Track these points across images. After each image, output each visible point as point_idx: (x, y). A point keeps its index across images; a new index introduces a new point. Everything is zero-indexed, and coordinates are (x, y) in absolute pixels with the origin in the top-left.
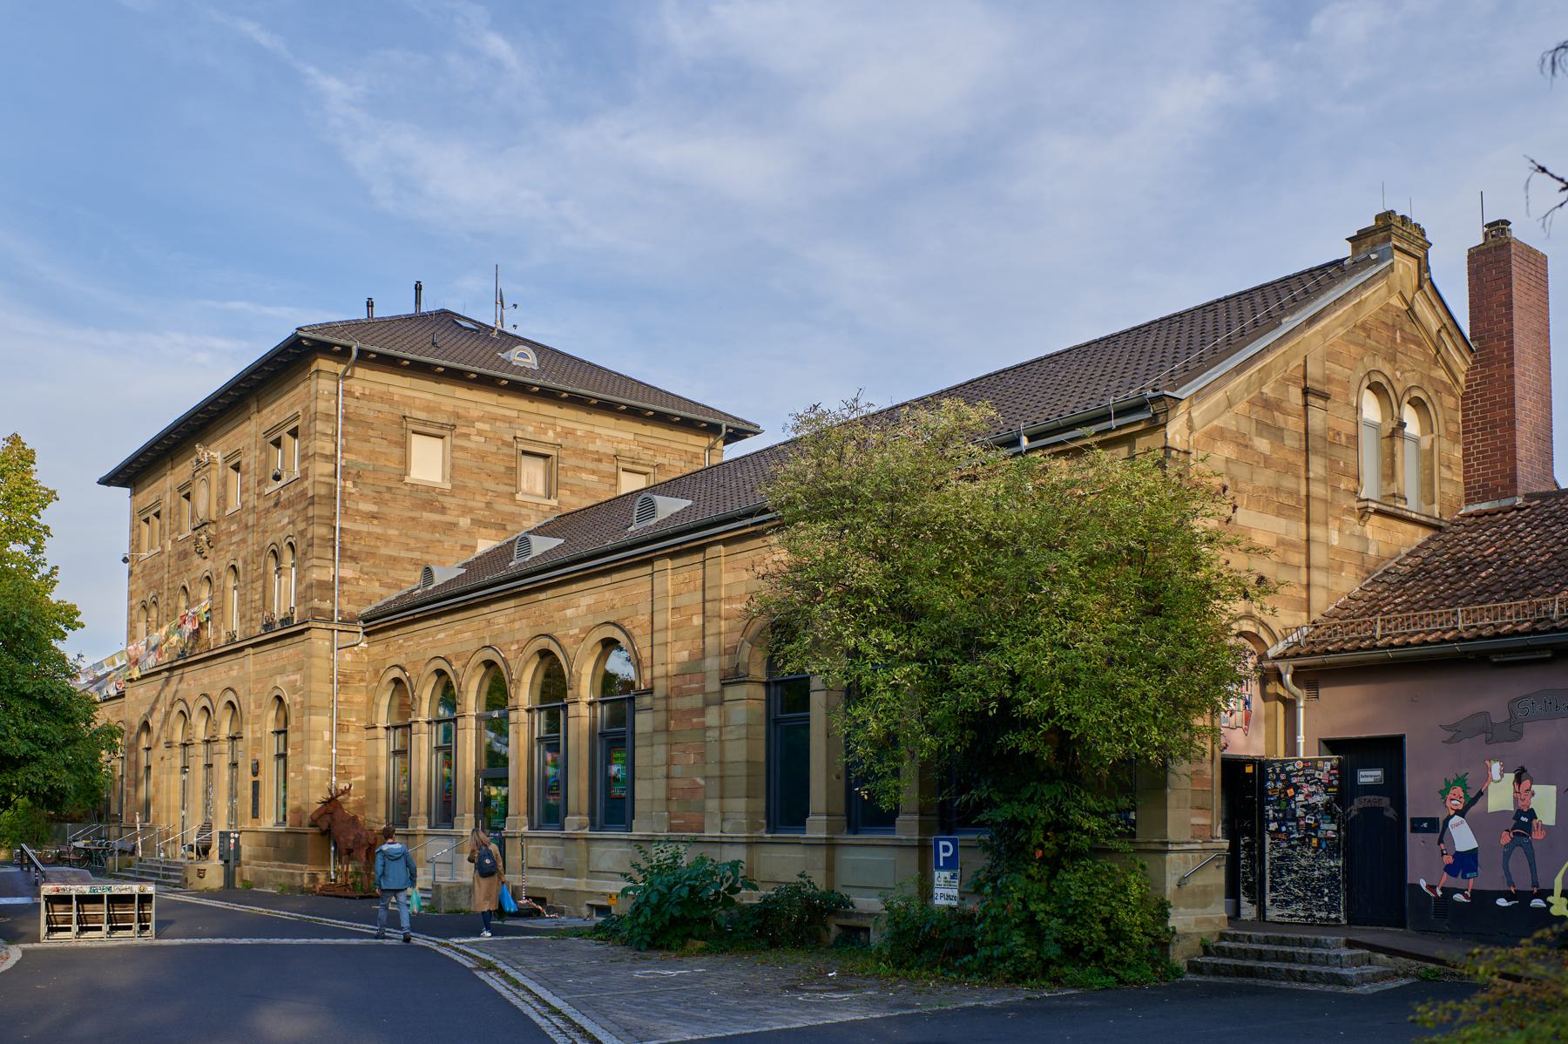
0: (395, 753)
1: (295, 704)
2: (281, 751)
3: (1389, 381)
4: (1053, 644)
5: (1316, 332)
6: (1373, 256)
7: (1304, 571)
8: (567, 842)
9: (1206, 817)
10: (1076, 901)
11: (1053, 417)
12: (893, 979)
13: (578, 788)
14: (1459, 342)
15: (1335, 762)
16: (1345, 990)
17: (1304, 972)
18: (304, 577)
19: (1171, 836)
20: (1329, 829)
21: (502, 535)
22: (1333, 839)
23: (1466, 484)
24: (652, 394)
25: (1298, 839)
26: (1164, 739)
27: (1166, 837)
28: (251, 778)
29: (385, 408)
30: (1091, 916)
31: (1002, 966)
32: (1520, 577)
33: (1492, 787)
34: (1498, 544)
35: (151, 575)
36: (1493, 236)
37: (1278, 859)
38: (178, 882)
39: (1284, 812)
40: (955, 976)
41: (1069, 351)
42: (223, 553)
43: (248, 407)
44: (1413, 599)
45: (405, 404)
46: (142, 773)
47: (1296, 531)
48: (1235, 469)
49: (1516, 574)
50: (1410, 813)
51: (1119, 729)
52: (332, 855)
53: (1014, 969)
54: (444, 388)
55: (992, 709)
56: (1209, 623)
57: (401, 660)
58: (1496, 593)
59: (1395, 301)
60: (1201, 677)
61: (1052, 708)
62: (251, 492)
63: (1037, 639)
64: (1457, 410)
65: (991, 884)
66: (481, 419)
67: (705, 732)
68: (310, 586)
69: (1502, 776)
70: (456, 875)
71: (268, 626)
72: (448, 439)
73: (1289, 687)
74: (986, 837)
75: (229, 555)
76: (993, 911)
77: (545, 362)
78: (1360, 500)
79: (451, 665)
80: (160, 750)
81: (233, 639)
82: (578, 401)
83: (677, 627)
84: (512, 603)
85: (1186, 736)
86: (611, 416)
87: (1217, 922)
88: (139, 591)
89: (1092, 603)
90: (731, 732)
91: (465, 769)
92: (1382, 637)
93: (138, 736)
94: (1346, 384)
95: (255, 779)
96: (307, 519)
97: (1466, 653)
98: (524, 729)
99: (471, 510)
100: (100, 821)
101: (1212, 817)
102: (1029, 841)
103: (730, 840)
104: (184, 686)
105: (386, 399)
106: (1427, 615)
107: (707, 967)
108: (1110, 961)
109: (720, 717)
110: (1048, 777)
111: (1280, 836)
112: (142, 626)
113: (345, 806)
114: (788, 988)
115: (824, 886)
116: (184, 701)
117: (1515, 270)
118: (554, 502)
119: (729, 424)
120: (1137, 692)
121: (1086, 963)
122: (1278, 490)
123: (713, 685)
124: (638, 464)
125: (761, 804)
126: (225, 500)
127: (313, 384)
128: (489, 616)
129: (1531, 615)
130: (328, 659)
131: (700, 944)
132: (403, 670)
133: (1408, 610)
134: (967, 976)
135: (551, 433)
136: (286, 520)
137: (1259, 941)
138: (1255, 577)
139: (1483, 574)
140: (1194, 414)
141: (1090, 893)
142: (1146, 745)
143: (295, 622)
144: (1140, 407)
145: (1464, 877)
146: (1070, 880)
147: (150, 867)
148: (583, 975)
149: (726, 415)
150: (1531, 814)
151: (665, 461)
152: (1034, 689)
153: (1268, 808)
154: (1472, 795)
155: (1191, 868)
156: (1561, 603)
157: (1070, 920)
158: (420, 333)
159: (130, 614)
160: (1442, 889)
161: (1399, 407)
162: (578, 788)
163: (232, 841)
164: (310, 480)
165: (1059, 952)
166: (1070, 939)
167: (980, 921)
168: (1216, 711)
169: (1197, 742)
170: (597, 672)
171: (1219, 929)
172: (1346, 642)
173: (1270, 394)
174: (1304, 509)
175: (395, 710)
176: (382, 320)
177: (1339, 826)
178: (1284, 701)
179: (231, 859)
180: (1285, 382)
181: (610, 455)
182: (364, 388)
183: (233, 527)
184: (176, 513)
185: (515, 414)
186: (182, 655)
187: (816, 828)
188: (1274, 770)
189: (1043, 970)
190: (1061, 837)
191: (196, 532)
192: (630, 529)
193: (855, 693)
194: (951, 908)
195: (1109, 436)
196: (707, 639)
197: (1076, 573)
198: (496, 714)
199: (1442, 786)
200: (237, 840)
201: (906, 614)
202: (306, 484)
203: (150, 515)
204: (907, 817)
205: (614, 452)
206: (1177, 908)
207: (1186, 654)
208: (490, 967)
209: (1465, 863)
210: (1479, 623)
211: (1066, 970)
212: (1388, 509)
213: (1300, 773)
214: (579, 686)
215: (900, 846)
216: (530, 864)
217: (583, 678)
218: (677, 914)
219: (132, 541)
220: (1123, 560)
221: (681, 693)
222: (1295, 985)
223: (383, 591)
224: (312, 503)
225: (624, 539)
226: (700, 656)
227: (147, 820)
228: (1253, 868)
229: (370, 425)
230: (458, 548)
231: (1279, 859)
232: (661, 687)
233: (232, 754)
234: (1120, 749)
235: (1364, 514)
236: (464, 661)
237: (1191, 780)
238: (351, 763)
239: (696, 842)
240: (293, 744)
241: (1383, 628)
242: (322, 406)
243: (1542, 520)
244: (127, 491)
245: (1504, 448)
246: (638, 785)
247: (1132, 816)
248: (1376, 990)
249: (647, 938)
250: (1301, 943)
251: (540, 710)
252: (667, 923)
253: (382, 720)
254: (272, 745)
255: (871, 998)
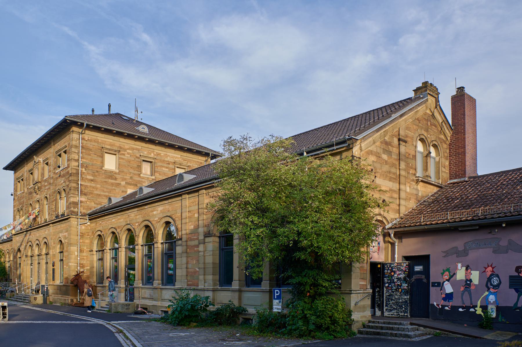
0: (99, 259)
1: (66, 243)
2: (62, 258)
3: (426, 138)
4: (312, 222)
5: (403, 120)
6: (421, 96)
7: (398, 200)
8: (154, 289)
9: (365, 282)
10: (320, 310)
11: (315, 145)
12: (258, 337)
13: (158, 271)
14: (448, 126)
15: (407, 264)
16: (409, 340)
17: (396, 334)
18: (68, 200)
19: (353, 288)
20: (405, 286)
21: (136, 188)
22: (406, 289)
23: (450, 173)
24: (187, 143)
25: (395, 289)
26: (350, 255)
27: (351, 288)
28: (52, 268)
29: (96, 144)
30: (325, 315)
31: (295, 332)
32: (468, 202)
33: (458, 272)
34: (460, 192)
35: (20, 200)
36: (459, 92)
37: (388, 296)
38: (27, 301)
39: (390, 280)
40: (279, 335)
41: (322, 127)
42: (43, 192)
43: (51, 144)
44: (433, 210)
45: (103, 143)
46: (18, 266)
47: (395, 186)
48: (376, 165)
49: (466, 202)
50: (432, 280)
51: (335, 251)
52: (78, 293)
53: (299, 333)
54: (116, 138)
55: (291, 244)
56: (366, 216)
57: (101, 229)
58: (460, 208)
59: (428, 112)
60: (364, 233)
61: (312, 244)
62: (52, 172)
63: (307, 220)
64: (447, 149)
65: (291, 304)
66: (129, 149)
67: (199, 253)
68: (70, 203)
69: (461, 268)
70: (119, 300)
71: (57, 217)
72: (117, 155)
73: (393, 239)
74: (291, 289)
75: (45, 193)
76: (292, 314)
77: (151, 131)
78: (416, 177)
79: (116, 230)
80: (24, 258)
81: (46, 221)
82: (161, 144)
83: (190, 217)
84: (136, 209)
85: (358, 254)
86: (173, 149)
87: (368, 317)
88: (17, 205)
89: (327, 208)
90: (207, 253)
91: (121, 265)
92: (423, 222)
93: (17, 253)
94: (412, 138)
95: (53, 268)
96: (69, 181)
97: (451, 227)
98: (140, 252)
99: (125, 179)
100: (6, 281)
101: (367, 282)
102: (304, 290)
103: (207, 289)
104: (31, 237)
105: (96, 141)
106: (438, 215)
107: (196, 332)
108: (332, 331)
109: (204, 248)
110: (311, 268)
111: (389, 288)
112: (18, 217)
113: (82, 277)
114: (221, 340)
115: (238, 304)
116: (31, 242)
117: (466, 103)
118: (153, 177)
119: (213, 153)
120: (341, 238)
121: (324, 331)
122: (390, 172)
123: (201, 237)
124: (182, 165)
125: (217, 277)
126: (43, 175)
127: (71, 135)
128: (129, 214)
129: (472, 215)
130: (77, 228)
131: (195, 324)
132: (101, 232)
133: (432, 213)
134: (283, 336)
135: (152, 154)
136: (63, 181)
137: (381, 323)
138: (382, 200)
139: (456, 202)
140: (362, 145)
141: (325, 308)
142: (344, 257)
143: (66, 215)
144: (344, 142)
145: (448, 301)
146: (318, 303)
147: (20, 297)
148: (153, 335)
149: (211, 150)
150: (471, 281)
151: (191, 165)
152: (306, 237)
153: (385, 279)
154: (452, 274)
155: (359, 299)
156: (481, 211)
157: (318, 317)
158: (109, 120)
159: (14, 213)
160: (441, 306)
161: (429, 147)
162: (158, 271)
163: (46, 288)
164: (70, 168)
165: (314, 327)
166: (318, 323)
167: (288, 317)
168: (368, 245)
169: (362, 257)
170: (164, 233)
171: (368, 319)
172: (412, 224)
173: (387, 140)
174: (398, 179)
175: (99, 245)
176: (96, 115)
177: (408, 285)
178: (391, 243)
179: (46, 294)
180: (392, 136)
181: (172, 162)
182: (89, 137)
183: (46, 184)
184: (28, 179)
185: (140, 148)
186: (30, 227)
187: (235, 285)
188: (387, 266)
189: (308, 334)
190: (316, 288)
191: (34, 185)
192: (175, 185)
193: (245, 238)
194: (279, 313)
195: (333, 152)
196: (199, 222)
197: (321, 197)
198: (131, 247)
199: (442, 272)
200: (47, 288)
201: (262, 211)
202: (69, 169)
203: (20, 180)
204: (265, 282)
205: (174, 161)
206: (354, 312)
207: (358, 226)
208: (121, 332)
209: (449, 297)
210: (455, 217)
211: (316, 333)
212: (425, 180)
213: (396, 267)
214: (158, 237)
215: (263, 292)
216: (143, 297)
217: (159, 235)
218: (187, 314)
219: (14, 189)
220: (337, 194)
221: (191, 240)
222: (393, 338)
223: (95, 205)
224: (71, 176)
225: (173, 187)
226: (197, 227)
227: (20, 281)
228: (380, 299)
229: (91, 150)
230: (121, 192)
231: (388, 296)
232: (184, 238)
233: (46, 259)
234: (335, 258)
235: (417, 181)
236: (121, 229)
237: (360, 269)
238: (85, 263)
239: (194, 290)
240: (65, 256)
241: (424, 219)
242: (74, 143)
243: (474, 185)
244: (13, 172)
245: (462, 162)
246: (177, 271)
247: (340, 281)
248: (420, 339)
249: (177, 322)
250: (395, 324)
251: (146, 245)
252: (183, 317)
253: (95, 248)
254: (58, 257)
255: (249, 343)
